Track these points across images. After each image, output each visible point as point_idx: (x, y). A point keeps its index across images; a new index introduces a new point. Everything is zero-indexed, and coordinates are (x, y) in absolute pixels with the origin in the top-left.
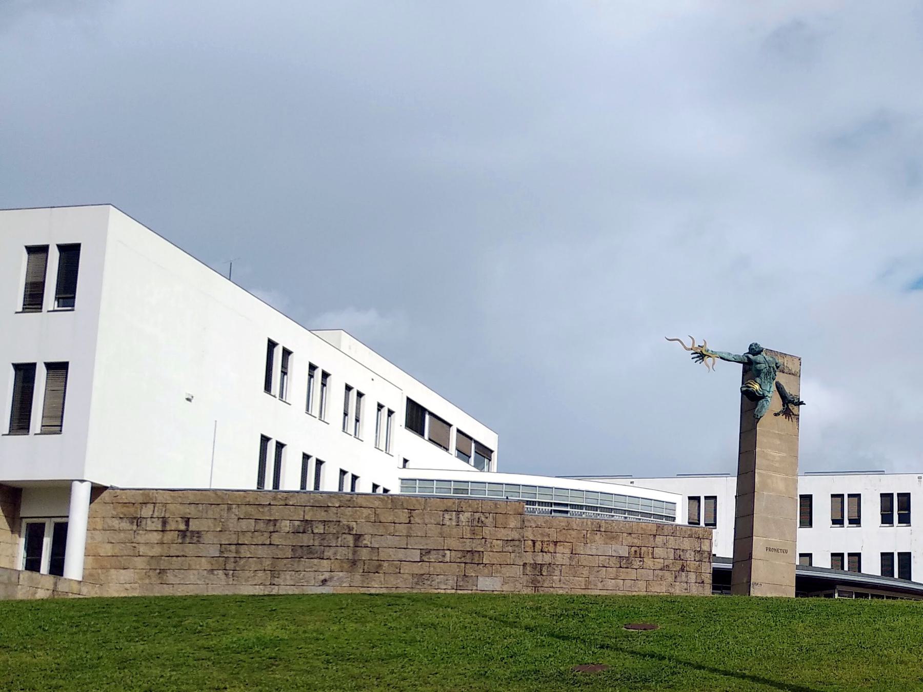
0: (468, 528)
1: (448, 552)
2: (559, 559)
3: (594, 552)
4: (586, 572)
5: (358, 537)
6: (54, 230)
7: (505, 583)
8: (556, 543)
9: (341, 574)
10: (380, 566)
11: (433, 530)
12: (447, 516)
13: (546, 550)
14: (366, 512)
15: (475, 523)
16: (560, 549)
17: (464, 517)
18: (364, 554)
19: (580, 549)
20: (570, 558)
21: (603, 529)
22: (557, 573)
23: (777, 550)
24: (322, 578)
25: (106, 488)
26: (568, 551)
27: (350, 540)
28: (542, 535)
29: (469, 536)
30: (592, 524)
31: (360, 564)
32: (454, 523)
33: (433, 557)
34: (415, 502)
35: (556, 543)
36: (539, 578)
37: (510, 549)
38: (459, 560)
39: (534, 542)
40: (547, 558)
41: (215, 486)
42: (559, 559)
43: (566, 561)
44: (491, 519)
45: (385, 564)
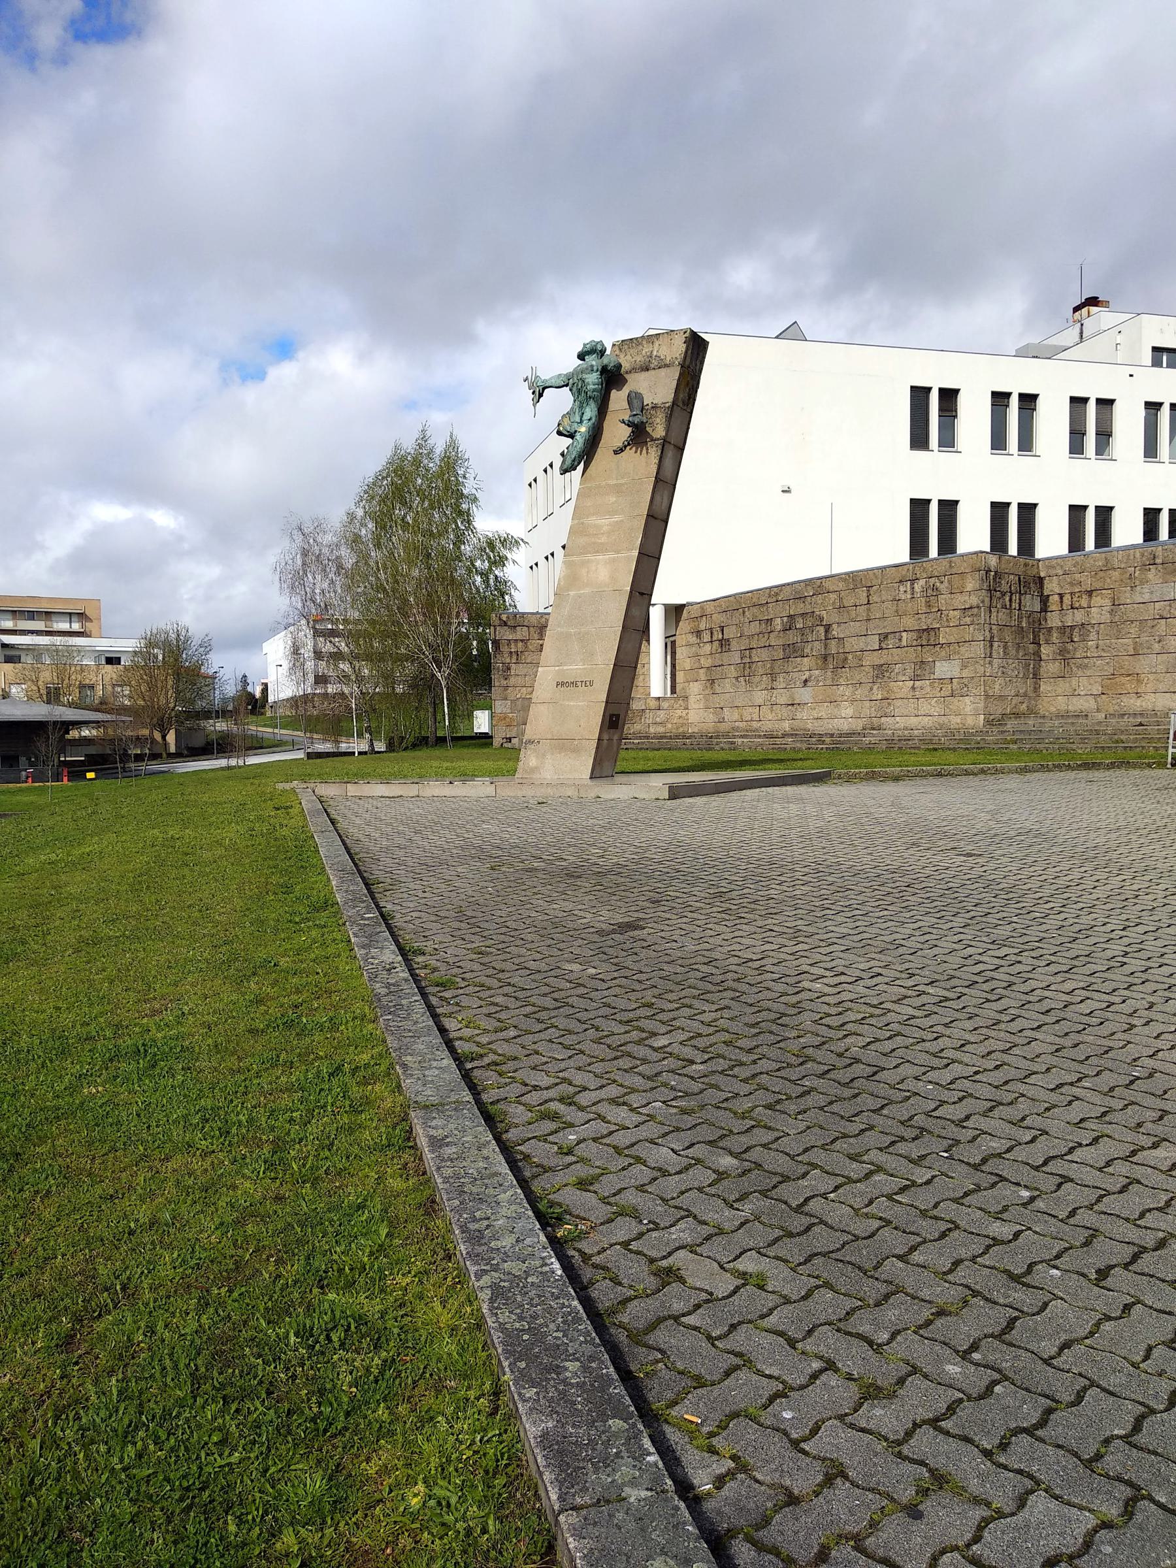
0: (923, 600)
1: (904, 634)
2: (1096, 615)
3: (1147, 597)
4: (1134, 630)
5: (828, 628)
6: (625, 312)
7: (964, 667)
8: (1090, 593)
9: (817, 672)
10: (846, 659)
11: (889, 608)
12: (902, 589)
13: (1077, 605)
14: (833, 596)
15: (930, 591)
16: (1097, 600)
17: (918, 587)
18: (833, 647)
19: (1126, 597)
20: (1111, 612)
21: (1158, 561)
22: (1093, 635)
23: (574, 684)
24: (804, 678)
25: (684, 605)
26: (1108, 602)
27: (822, 629)
28: (1072, 584)
29: (924, 610)
30: (1143, 555)
31: (830, 659)
32: (909, 596)
33: (891, 642)
34: (872, 576)
35: (1090, 593)
36: (1070, 646)
37: (968, 620)
38: (915, 643)
39: (1061, 596)
40: (1079, 617)
41: (845, 564)
42: (1096, 615)
43: (1106, 617)
44: (946, 584)
45: (850, 657)
